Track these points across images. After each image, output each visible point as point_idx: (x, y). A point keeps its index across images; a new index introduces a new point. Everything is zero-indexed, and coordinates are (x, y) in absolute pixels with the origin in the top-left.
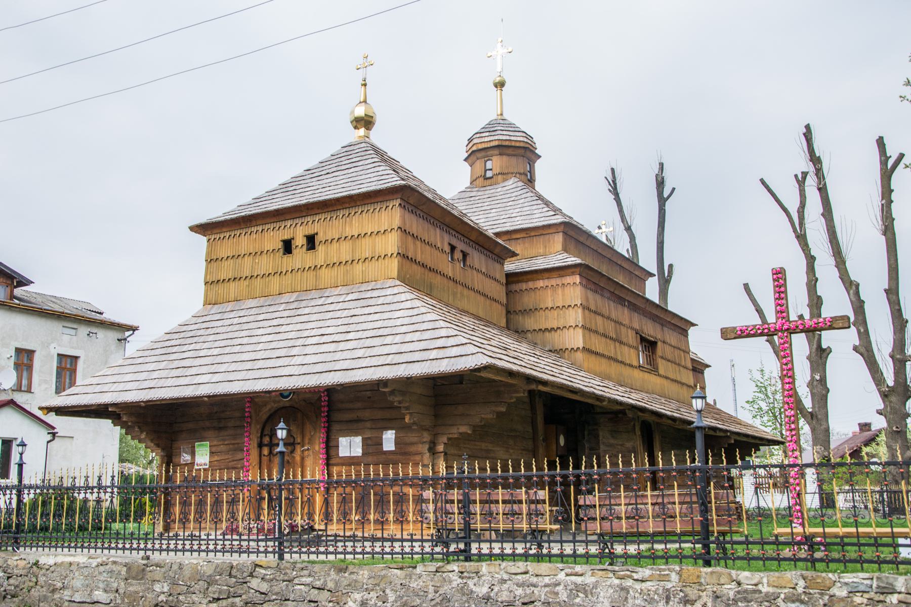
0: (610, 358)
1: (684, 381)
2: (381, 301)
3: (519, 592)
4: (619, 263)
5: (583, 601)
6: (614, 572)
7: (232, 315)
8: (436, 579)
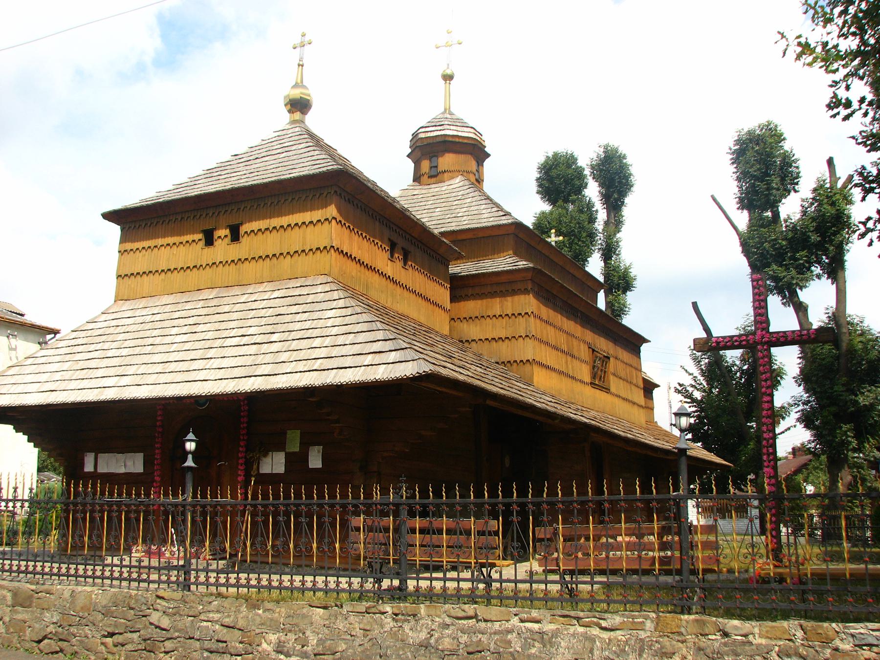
0: (561, 373)
1: (635, 400)
2: (310, 299)
3: (464, 638)
4: (571, 271)
5: (540, 652)
6: (578, 619)
7: (144, 312)
8: (365, 621)
